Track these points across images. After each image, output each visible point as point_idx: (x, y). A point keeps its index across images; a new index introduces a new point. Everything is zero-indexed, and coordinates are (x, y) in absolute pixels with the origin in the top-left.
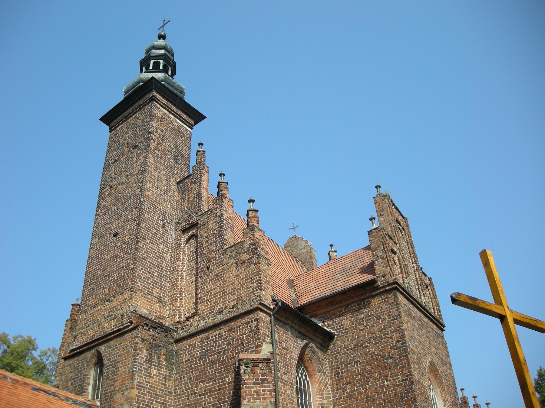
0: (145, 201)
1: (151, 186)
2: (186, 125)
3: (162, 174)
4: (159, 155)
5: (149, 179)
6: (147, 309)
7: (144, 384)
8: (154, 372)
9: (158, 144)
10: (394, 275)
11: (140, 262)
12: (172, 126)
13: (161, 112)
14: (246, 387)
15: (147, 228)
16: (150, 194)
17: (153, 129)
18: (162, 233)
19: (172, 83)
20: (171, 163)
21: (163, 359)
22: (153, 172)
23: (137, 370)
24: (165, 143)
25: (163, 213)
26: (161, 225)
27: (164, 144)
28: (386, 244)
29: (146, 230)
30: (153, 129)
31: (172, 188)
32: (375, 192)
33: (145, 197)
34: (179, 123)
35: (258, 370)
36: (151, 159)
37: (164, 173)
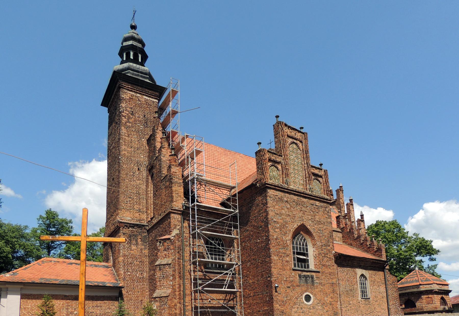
0: (122, 158)
1: (126, 147)
2: (152, 98)
3: (134, 138)
4: (130, 126)
5: (124, 143)
6: (131, 217)
7: (127, 254)
8: (134, 247)
9: (129, 118)
10: (265, 179)
11: (122, 194)
12: (140, 102)
13: (128, 95)
14: (160, 253)
15: (126, 173)
16: (126, 152)
17: (123, 109)
18: (138, 174)
19: (136, 69)
20: (141, 129)
21: (139, 240)
22: (127, 138)
23: (122, 248)
24: (134, 116)
25: (138, 162)
26: (137, 169)
27: (134, 117)
28: (263, 160)
29: (125, 175)
30: (123, 109)
31: (143, 144)
32: (274, 121)
33: (122, 155)
34: (146, 99)
35: (166, 244)
36: (124, 130)
37: (136, 136)
